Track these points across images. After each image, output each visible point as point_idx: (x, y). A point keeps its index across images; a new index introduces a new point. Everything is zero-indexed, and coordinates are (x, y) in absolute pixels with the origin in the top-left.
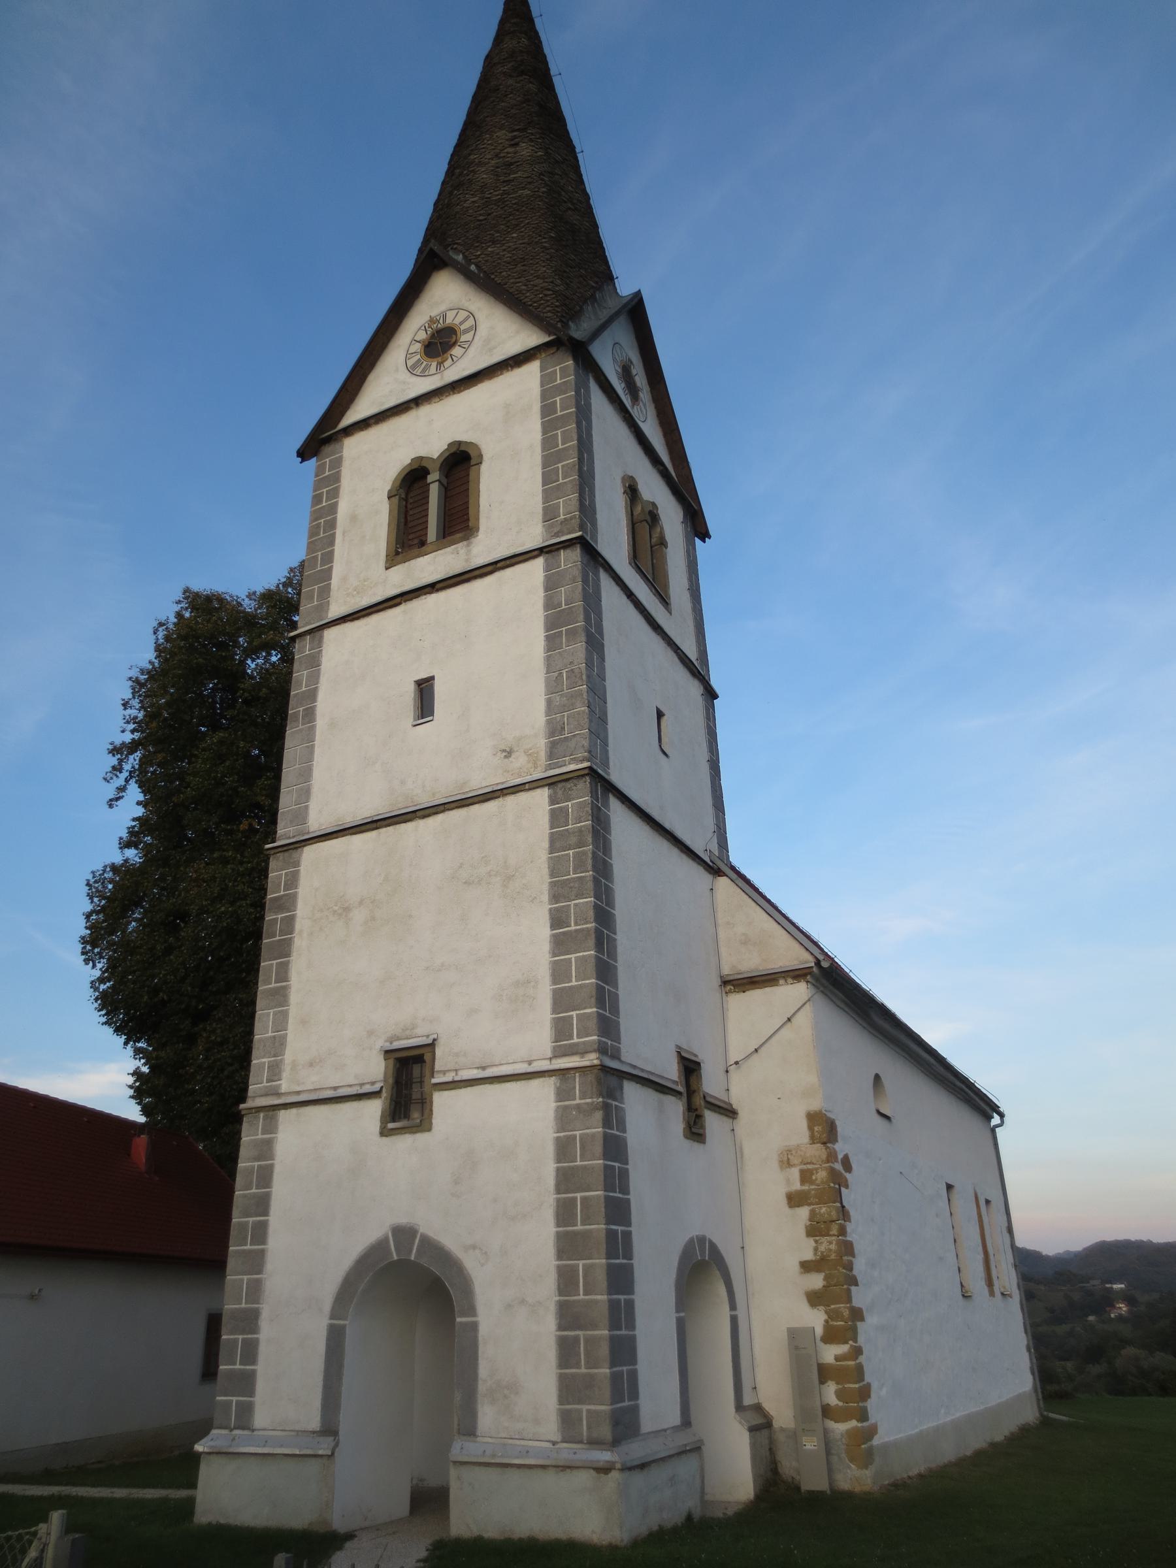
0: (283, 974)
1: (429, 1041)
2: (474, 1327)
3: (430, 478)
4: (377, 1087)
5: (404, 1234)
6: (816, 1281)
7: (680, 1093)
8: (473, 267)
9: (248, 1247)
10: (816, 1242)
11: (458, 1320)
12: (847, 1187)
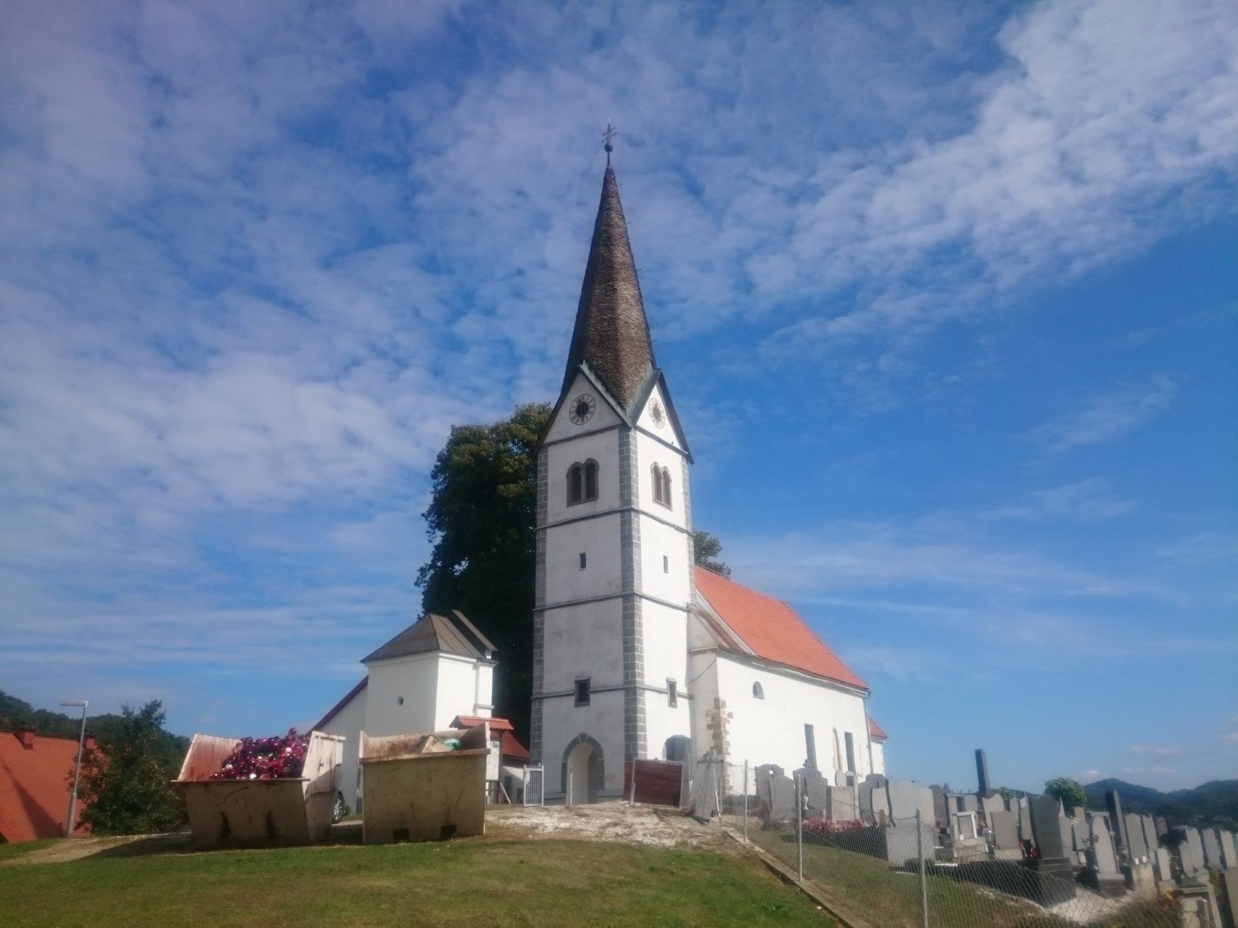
0: (541, 654)
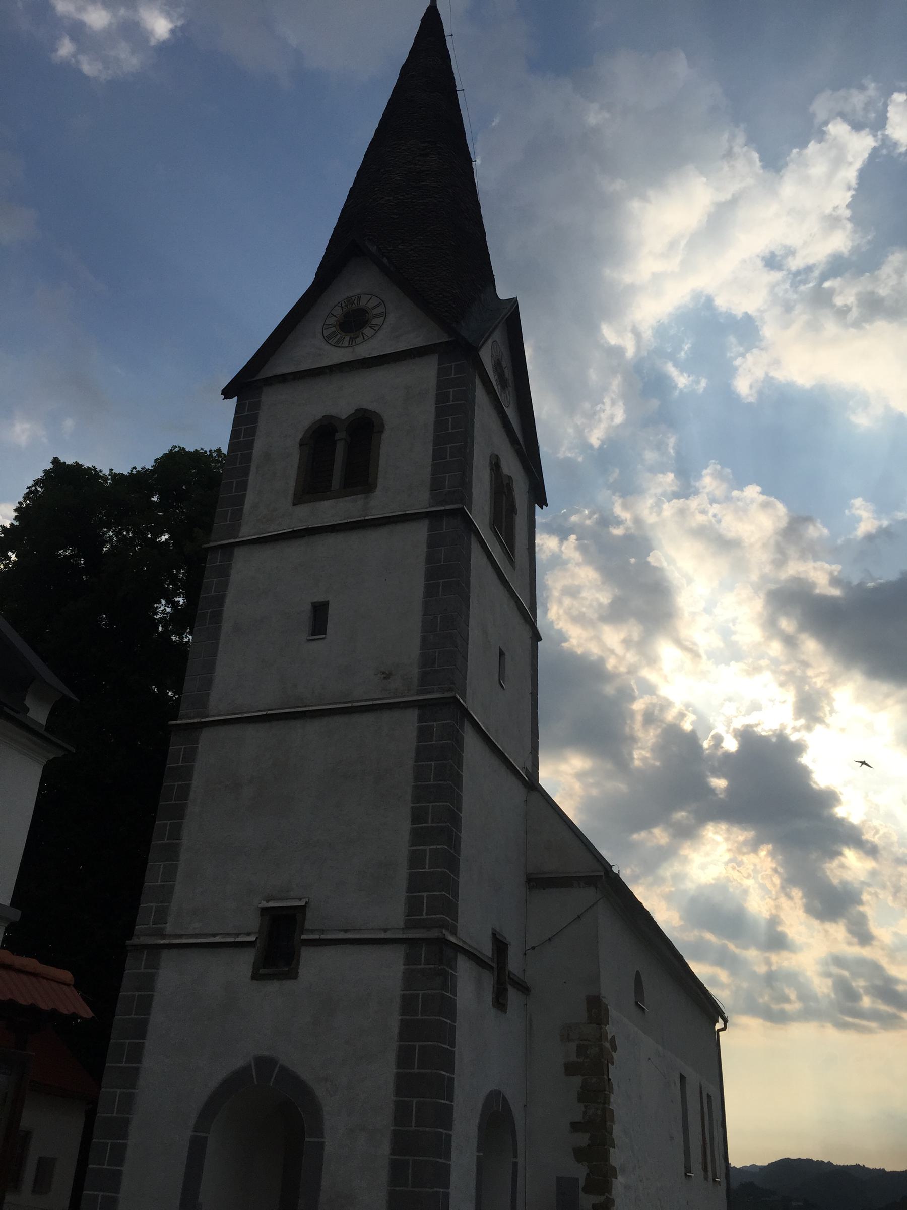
1: (302, 903)
2: (321, 1145)
3: (338, 436)
4: (252, 938)
5: (265, 1064)
6: (583, 1140)
7: (492, 968)
8: (385, 260)
9: (123, 1065)
10: (586, 1107)
11: (307, 1140)
12: (613, 1064)
